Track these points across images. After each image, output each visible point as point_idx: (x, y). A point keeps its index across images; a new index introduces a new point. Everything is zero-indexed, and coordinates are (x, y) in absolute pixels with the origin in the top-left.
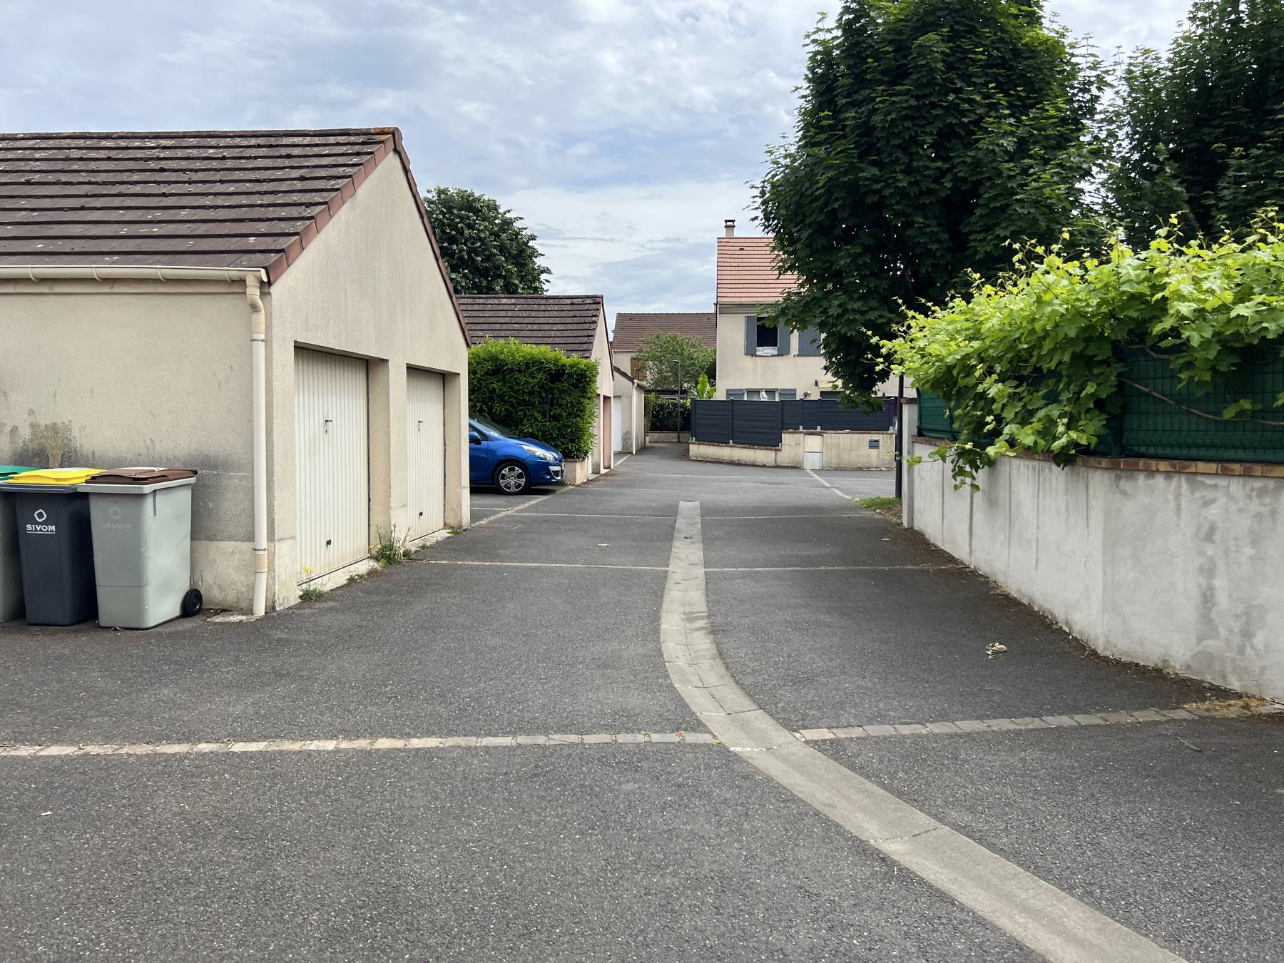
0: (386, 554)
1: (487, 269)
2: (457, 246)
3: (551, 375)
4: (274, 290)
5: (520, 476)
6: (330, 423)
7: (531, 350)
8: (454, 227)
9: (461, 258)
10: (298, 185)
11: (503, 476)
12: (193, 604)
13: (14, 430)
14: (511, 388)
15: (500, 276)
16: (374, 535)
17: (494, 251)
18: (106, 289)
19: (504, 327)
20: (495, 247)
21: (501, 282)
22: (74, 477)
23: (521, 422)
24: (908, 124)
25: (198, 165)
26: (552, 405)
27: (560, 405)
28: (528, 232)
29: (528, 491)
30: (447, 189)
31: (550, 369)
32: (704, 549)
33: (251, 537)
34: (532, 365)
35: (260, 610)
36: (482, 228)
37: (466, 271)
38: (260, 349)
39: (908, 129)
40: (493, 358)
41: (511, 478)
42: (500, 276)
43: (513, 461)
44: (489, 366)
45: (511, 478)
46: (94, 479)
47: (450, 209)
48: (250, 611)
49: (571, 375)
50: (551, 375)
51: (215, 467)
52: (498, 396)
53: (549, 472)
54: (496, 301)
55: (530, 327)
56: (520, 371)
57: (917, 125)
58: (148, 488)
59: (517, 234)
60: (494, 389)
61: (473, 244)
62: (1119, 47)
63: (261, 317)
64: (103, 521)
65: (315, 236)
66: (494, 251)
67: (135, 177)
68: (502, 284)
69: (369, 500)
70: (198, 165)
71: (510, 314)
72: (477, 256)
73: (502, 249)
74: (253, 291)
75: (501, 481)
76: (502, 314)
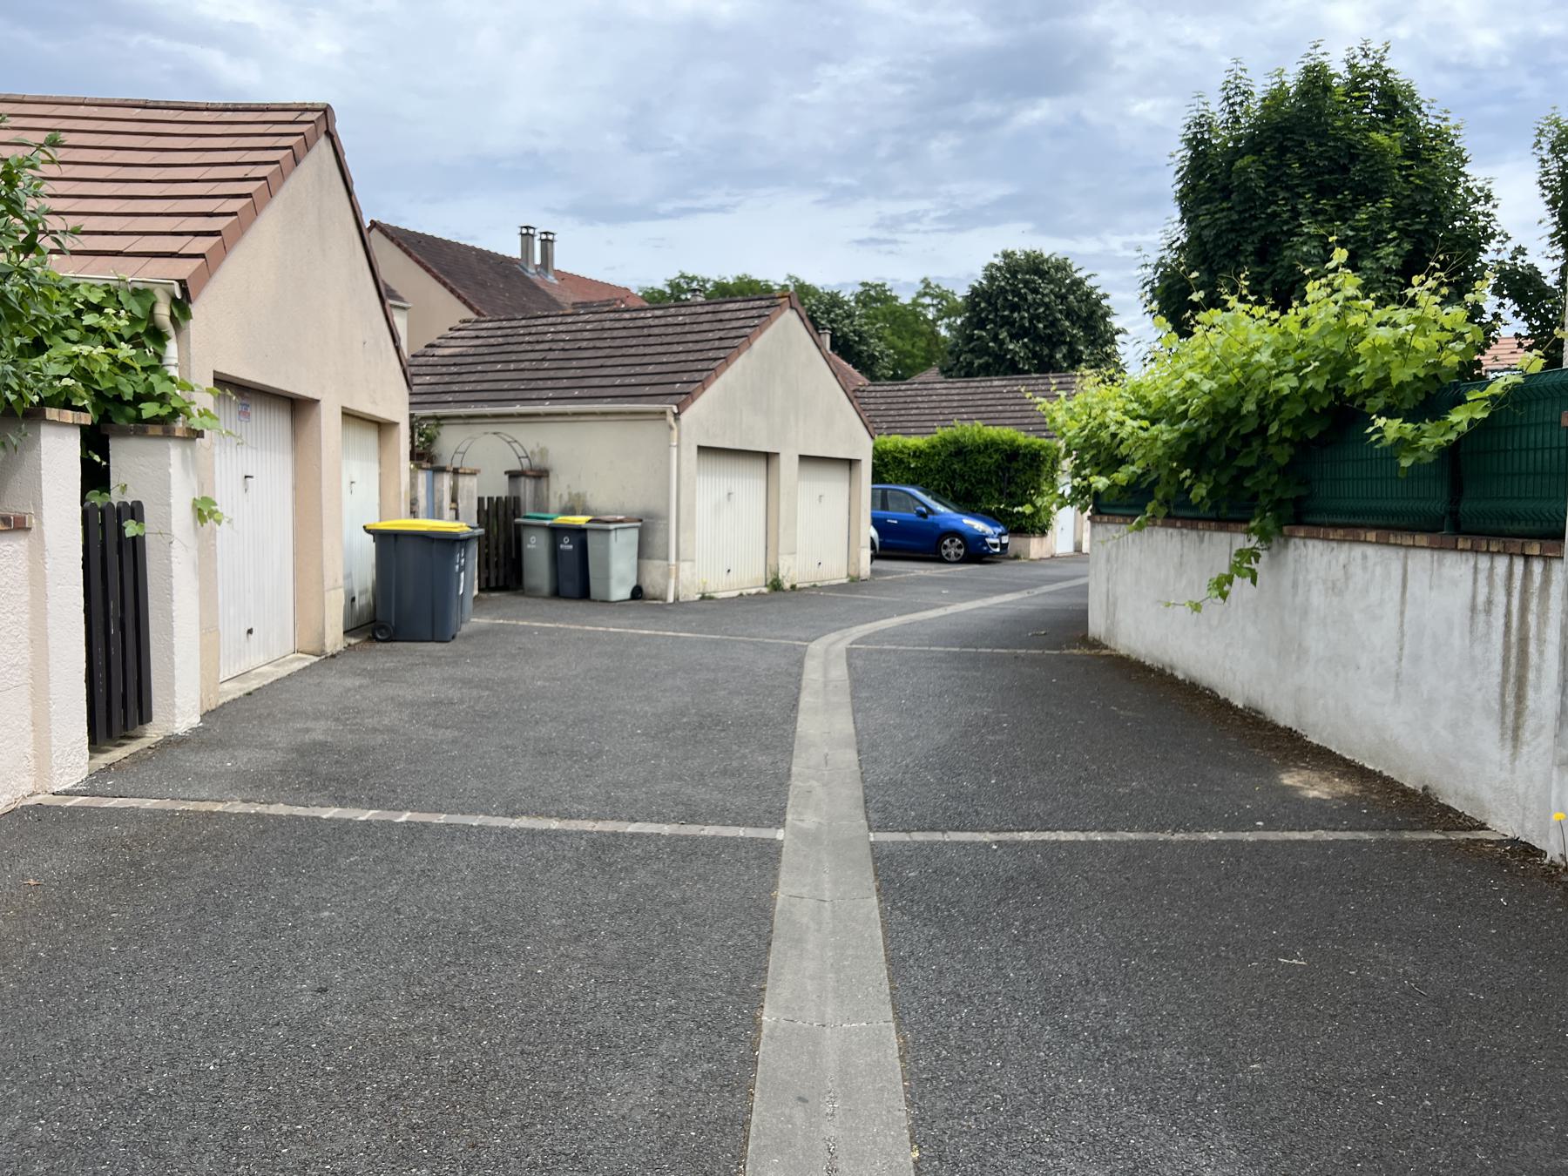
0: (776, 586)
1: (1050, 336)
2: (1019, 313)
3: (1007, 455)
4: (683, 417)
5: (959, 547)
6: (248, 479)
7: (993, 432)
8: (1016, 293)
9: (1022, 326)
10: (717, 344)
11: (945, 547)
12: (637, 593)
13: (561, 496)
14: (971, 467)
15: (1064, 343)
16: (769, 575)
17: (1059, 316)
18: (603, 418)
19: (990, 409)
20: (1061, 311)
21: (1064, 349)
22: (580, 520)
23: (979, 499)
24: (1233, 236)
25: (670, 330)
26: (1009, 483)
27: (1016, 484)
28: (1100, 291)
29: (967, 559)
30: (1013, 253)
31: (1006, 450)
32: (51, 407)
33: (667, 558)
34: (991, 446)
35: (671, 599)
36: (1046, 291)
37: (1026, 340)
38: (674, 451)
39: (1232, 240)
40: (956, 441)
41: (952, 548)
42: (1064, 343)
43: (955, 533)
44: (952, 448)
45: (952, 548)
46: (590, 521)
47: (1014, 275)
48: (665, 600)
49: (1025, 455)
50: (1007, 455)
51: (652, 518)
52: (960, 475)
53: (985, 544)
54: (989, 384)
55: (1012, 408)
56: (979, 452)
57: (1241, 236)
58: (612, 526)
59: (1088, 295)
60: (955, 469)
61: (1036, 309)
62: (1554, 108)
63: (675, 433)
64: (593, 541)
65: (714, 381)
66: (1059, 316)
67: (634, 342)
68: (1064, 351)
69: (766, 548)
70: (670, 330)
71: (998, 396)
72: (1039, 322)
73: (1069, 314)
74: (671, 419)
75: (943, 551)
76: (990, 396)
